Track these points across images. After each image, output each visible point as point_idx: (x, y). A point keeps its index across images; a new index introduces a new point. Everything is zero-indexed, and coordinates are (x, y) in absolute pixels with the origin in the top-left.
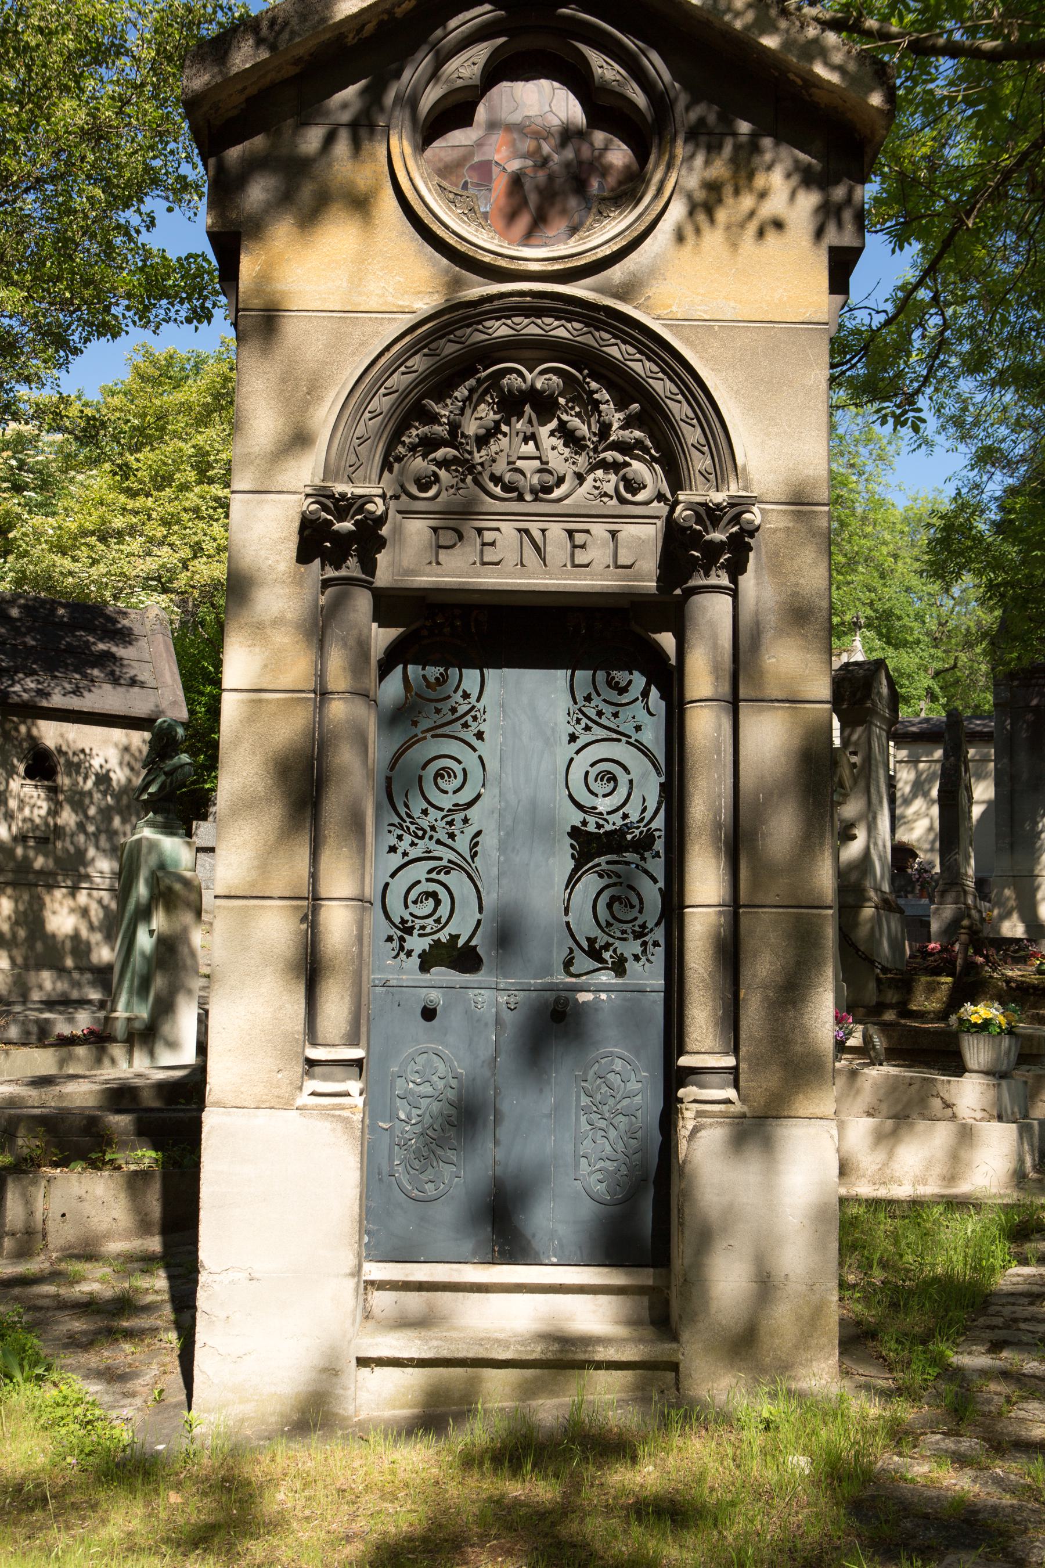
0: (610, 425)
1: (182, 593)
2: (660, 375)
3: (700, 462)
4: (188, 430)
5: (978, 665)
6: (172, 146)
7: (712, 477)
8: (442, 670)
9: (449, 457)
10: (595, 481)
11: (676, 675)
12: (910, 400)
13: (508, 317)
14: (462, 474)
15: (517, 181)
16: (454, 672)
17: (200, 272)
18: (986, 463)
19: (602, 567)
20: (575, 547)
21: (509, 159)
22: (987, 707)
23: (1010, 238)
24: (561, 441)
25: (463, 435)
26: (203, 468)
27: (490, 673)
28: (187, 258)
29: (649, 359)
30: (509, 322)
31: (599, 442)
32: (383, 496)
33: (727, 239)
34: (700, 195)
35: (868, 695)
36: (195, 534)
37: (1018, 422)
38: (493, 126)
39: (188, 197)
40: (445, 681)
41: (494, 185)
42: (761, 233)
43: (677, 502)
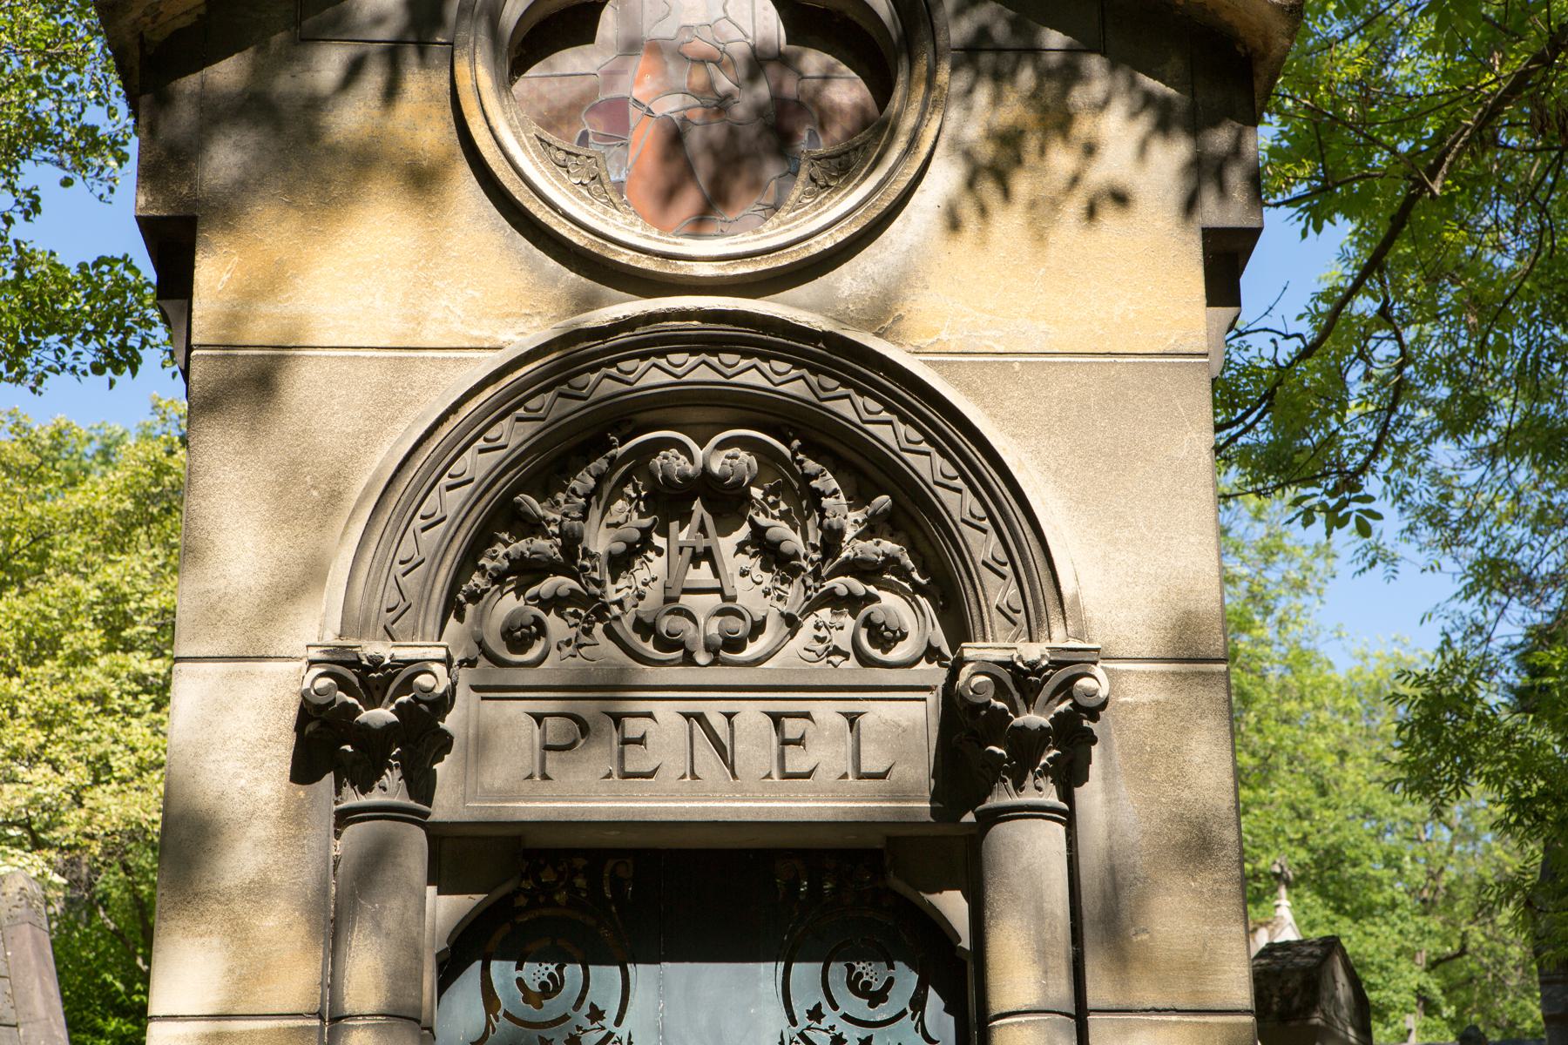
0: (840, 533)
1: (70, 848)
2: (924, 446)
3: (998, 592)
4: (91, 557)
5: (1506, 942)
6: (72, 77)
7: (1021, 617)
8: (552, 968)
9: (563, 591)
10: (817, 627)
11: (971, 968)
12: (1350, 482)
13: (662, 354)
14: (586, 620)
15: (675, 138)
16: (573, 972)
17: (121, 287)
18: (1491, 589)
19: (834, 776)
20: (785, 742)
21: (660, 94)
22: (1528, 1025)
23: (1506, 210)
24: (757, 561)
25: (587, 554)
26: (115, 625)
27: (641, 973)
28: (96, 264)
29: (905, 420)
30: (663, 362)
31: (823, 561)
32: (447, 661)
33: (1031, 223)
34: (986, 152)
35: (1312, 1004)
36: (97, 740)
37: (1541, 515)
38: (631, 47)
39: (98, 162)
40: (558, 988)
41: (632, 138)
42: (1091, 212)
43: (960, 662)
